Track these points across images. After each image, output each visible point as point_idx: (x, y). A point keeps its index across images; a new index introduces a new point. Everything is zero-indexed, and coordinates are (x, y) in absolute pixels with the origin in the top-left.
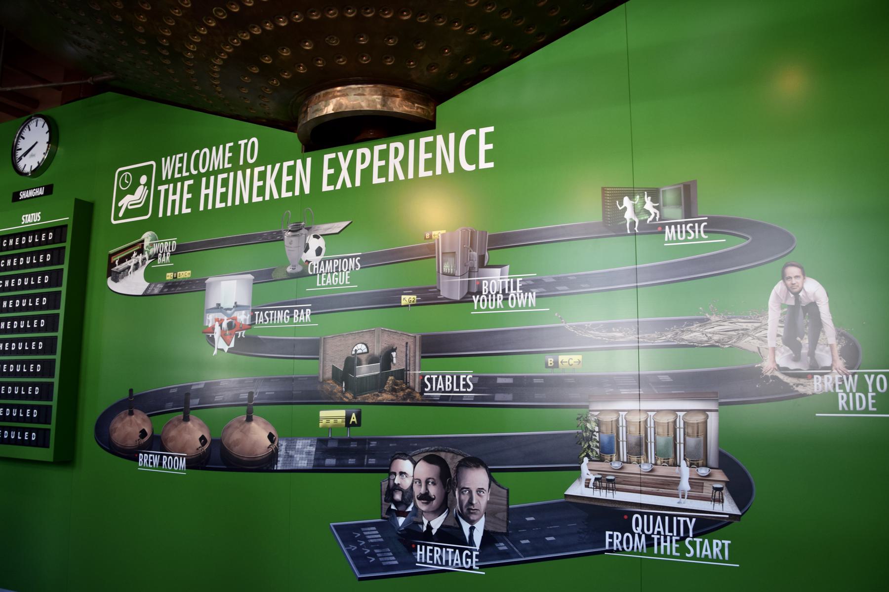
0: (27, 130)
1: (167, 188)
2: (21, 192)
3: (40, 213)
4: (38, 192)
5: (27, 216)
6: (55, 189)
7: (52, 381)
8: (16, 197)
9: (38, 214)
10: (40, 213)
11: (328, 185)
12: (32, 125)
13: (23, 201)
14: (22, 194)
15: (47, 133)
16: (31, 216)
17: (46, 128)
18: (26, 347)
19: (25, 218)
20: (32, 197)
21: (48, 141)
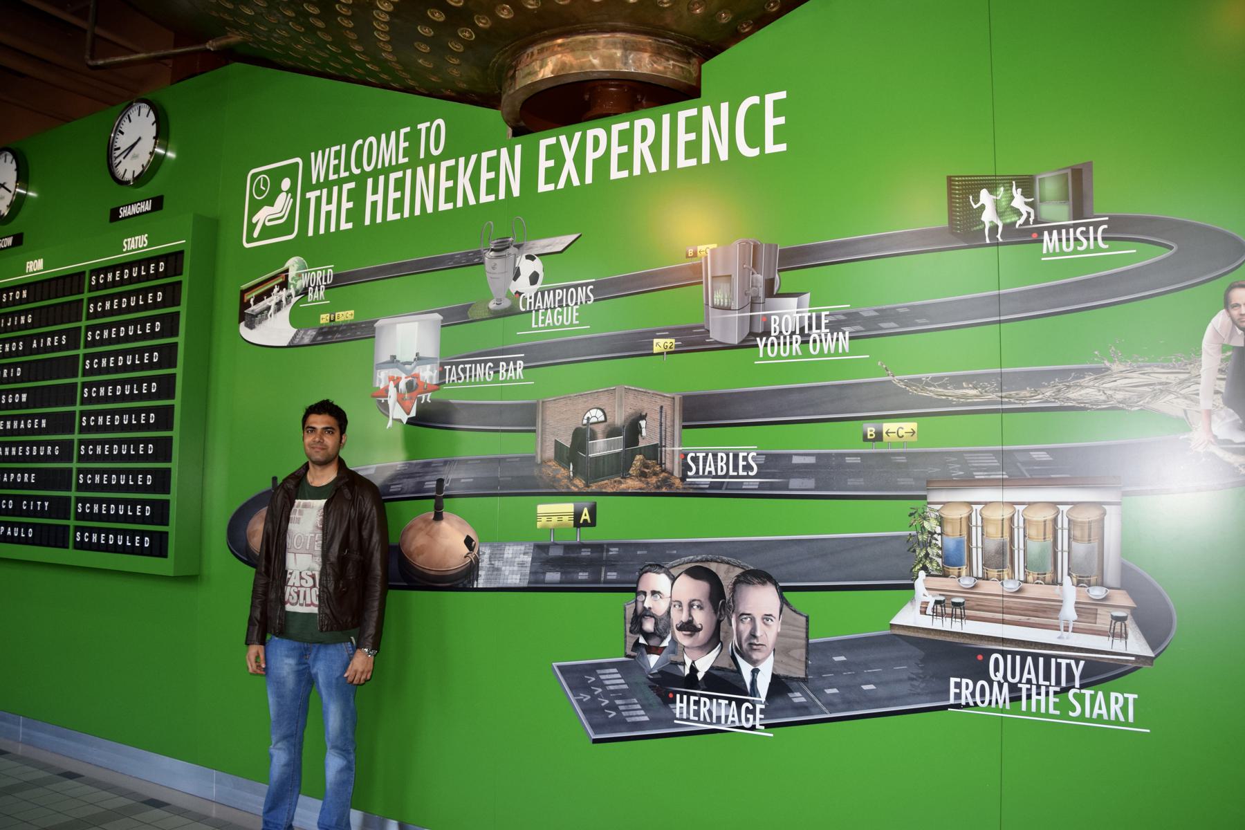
0: (127, 121)
3: (146, 235)
8: (115, 215)
10: (146, 235)
12: (133, 113)
14: (122, 211)
17: (152, 117)
19: (127, 243)
21: (154, 135)
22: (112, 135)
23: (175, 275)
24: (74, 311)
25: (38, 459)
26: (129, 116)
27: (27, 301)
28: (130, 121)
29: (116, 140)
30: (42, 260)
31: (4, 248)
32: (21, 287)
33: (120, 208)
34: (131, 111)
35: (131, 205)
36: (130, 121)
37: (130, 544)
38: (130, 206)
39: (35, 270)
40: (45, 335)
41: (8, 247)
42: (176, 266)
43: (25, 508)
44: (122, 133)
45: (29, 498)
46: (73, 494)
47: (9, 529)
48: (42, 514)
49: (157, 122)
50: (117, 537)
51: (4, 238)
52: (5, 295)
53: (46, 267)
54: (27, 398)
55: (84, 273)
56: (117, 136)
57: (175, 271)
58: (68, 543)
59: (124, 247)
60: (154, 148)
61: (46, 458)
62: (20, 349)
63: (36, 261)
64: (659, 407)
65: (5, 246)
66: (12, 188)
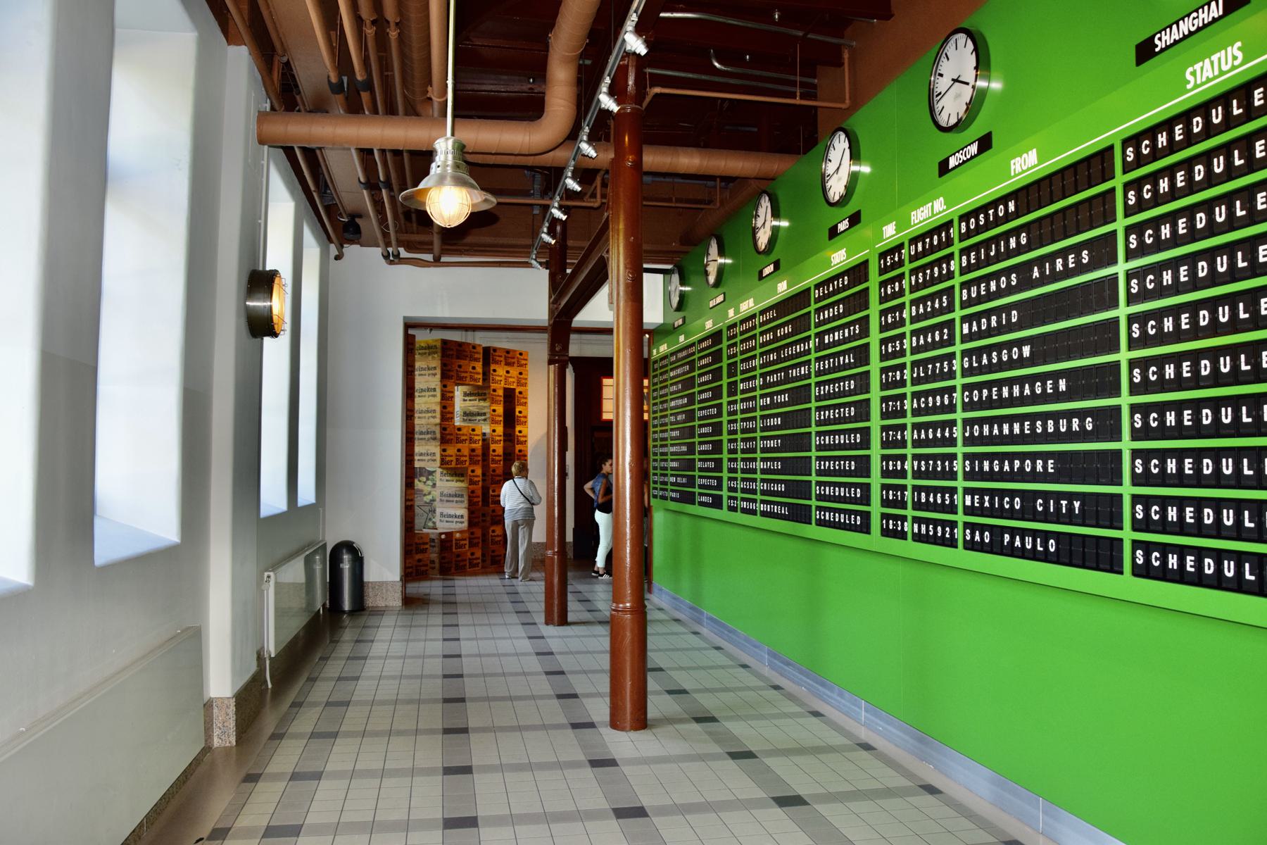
0: (833, 149)
1: (1235, 62)
2: (1158, 35)
3: (1239, 44)
4: (1205, 15)
5: (1198, 66)
6: (935, 169)
7: (954, 418)
8: (944, 168)
9: (751, 300)
10: (1239, 44)
11: (1116, 231)
12: (950, 49)
13: (766, 278)
14: (1160, 39)
15: (972, 53)
16: (1212, 63)
17: (970, 45)
18: (974, 362)
19: (1194, 74)
20: (1191, 33)
21: (975, 65)
22: (932, 79)
23: (1104, 181)
24: (1102, 209)
25: (1057, 437)
26: (946, 54)
27: (1017, 215)
28: (948, 59)
29: (936, 85)
30: (1035, 150)
31: (968, 160)
32: (1004, 200)
33: (1154, 36)
34: (947, 47)
35: (1177, 23)
36: (948, 59)
37: (1041, 549)
38: (1174, 27)
39: (1025, 168)
40: (1051, 257)
41: (972, 157)
42: (1103, 168)
43: (1040, 509)
44: (941, 75)
45: (1046, 495)
46: (697, 490)
47: (1018, 538)
48: (1070, 519)
49: (976, 49)
50: (1025, 539)
51: (966, 147)
52: (982, 215)
53: (668, 348)
54: (1031, 352)
55: (1111, 148)
56: (937, 81)
57: (1040, 202)
58: (1121, 565)
59: (1189, 82)
60: (976, 81)
61: (1070, 437)
62: (945, 305)
63: (1025, 155)
64: (437, 485)
65: (968, 157)
66: (971, 80)
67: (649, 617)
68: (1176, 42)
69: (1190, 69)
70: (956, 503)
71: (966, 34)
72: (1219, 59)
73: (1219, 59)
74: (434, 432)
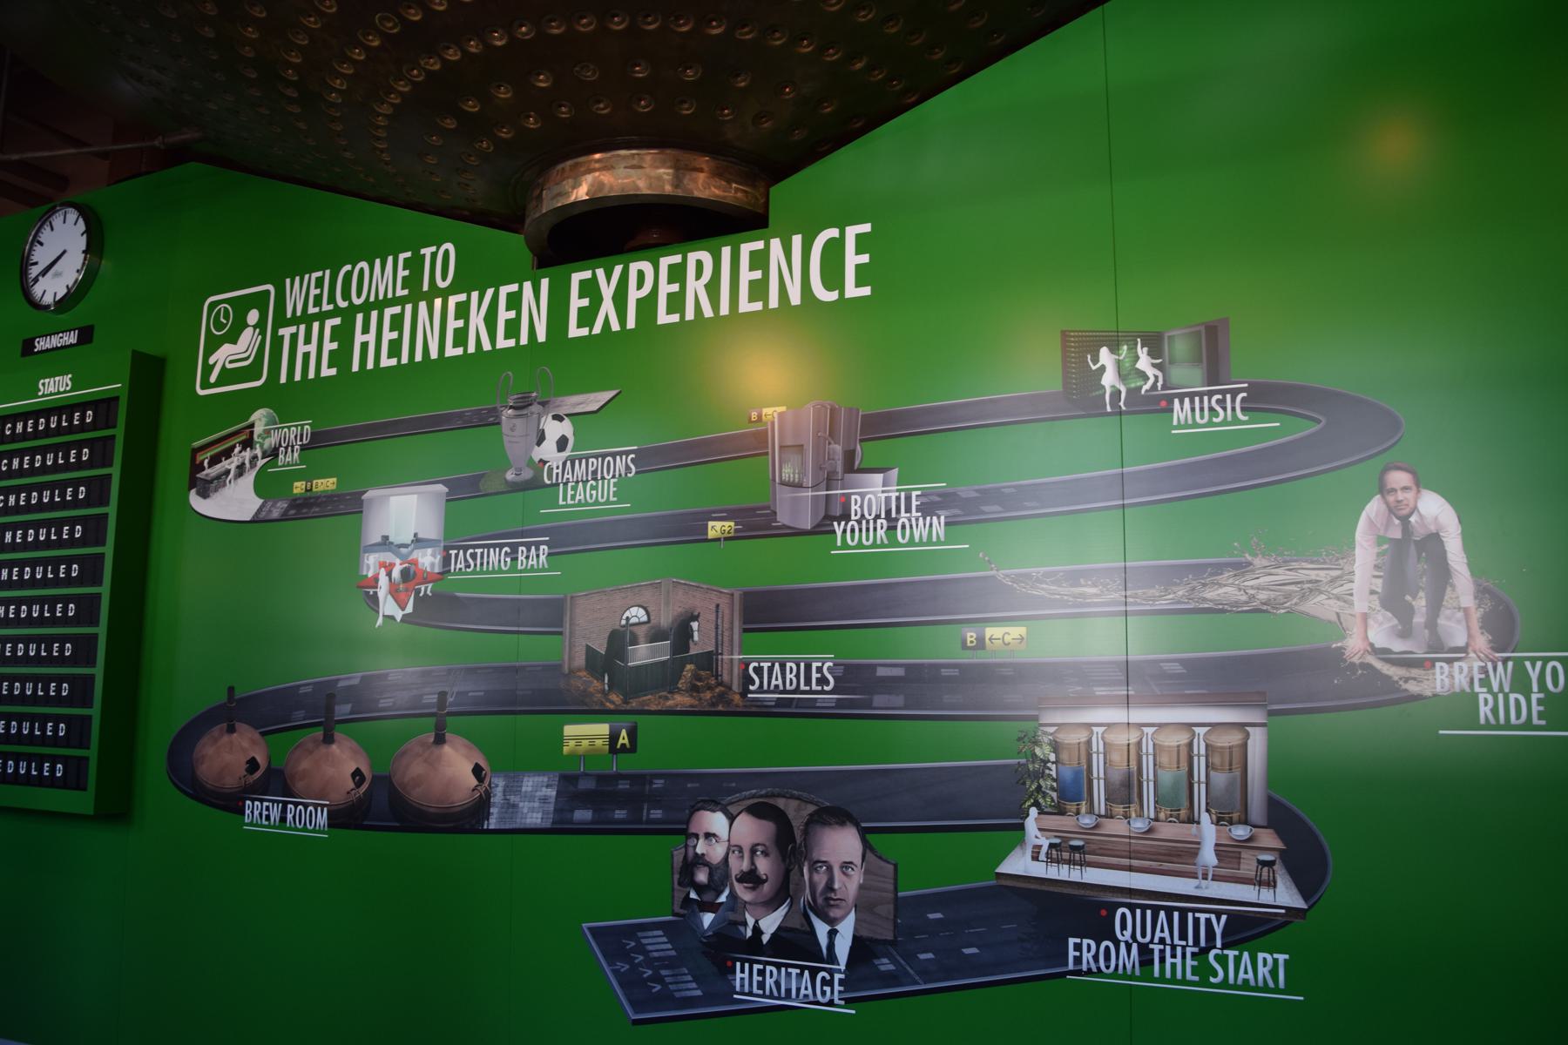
0: (48, 229)
2: (38, 340)
3: (70, 376)
4: (67, 338)
5: (47, 381)
8: (28, 347)
9: (67, 378)
10: (70, 376)
12: (57, 220)
14: (38, 342)
15: (82, 235)
16: (55, 382)
19: (44, 384)
20: (57, 348)
59: (40, 390)
67: (1444, 603)
68: (47, 350)
69: (42, 381)
70: (482, 693)
71: (78, 211)
72: (59, 381)
73: (59, 381)
74: (1379, 529)
